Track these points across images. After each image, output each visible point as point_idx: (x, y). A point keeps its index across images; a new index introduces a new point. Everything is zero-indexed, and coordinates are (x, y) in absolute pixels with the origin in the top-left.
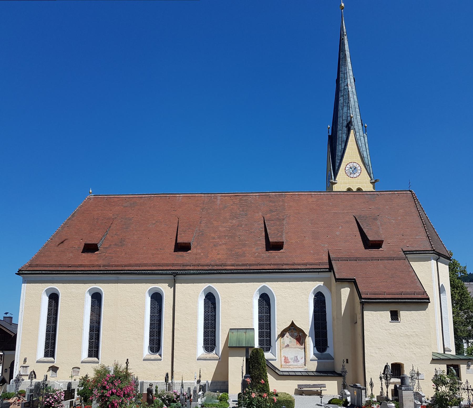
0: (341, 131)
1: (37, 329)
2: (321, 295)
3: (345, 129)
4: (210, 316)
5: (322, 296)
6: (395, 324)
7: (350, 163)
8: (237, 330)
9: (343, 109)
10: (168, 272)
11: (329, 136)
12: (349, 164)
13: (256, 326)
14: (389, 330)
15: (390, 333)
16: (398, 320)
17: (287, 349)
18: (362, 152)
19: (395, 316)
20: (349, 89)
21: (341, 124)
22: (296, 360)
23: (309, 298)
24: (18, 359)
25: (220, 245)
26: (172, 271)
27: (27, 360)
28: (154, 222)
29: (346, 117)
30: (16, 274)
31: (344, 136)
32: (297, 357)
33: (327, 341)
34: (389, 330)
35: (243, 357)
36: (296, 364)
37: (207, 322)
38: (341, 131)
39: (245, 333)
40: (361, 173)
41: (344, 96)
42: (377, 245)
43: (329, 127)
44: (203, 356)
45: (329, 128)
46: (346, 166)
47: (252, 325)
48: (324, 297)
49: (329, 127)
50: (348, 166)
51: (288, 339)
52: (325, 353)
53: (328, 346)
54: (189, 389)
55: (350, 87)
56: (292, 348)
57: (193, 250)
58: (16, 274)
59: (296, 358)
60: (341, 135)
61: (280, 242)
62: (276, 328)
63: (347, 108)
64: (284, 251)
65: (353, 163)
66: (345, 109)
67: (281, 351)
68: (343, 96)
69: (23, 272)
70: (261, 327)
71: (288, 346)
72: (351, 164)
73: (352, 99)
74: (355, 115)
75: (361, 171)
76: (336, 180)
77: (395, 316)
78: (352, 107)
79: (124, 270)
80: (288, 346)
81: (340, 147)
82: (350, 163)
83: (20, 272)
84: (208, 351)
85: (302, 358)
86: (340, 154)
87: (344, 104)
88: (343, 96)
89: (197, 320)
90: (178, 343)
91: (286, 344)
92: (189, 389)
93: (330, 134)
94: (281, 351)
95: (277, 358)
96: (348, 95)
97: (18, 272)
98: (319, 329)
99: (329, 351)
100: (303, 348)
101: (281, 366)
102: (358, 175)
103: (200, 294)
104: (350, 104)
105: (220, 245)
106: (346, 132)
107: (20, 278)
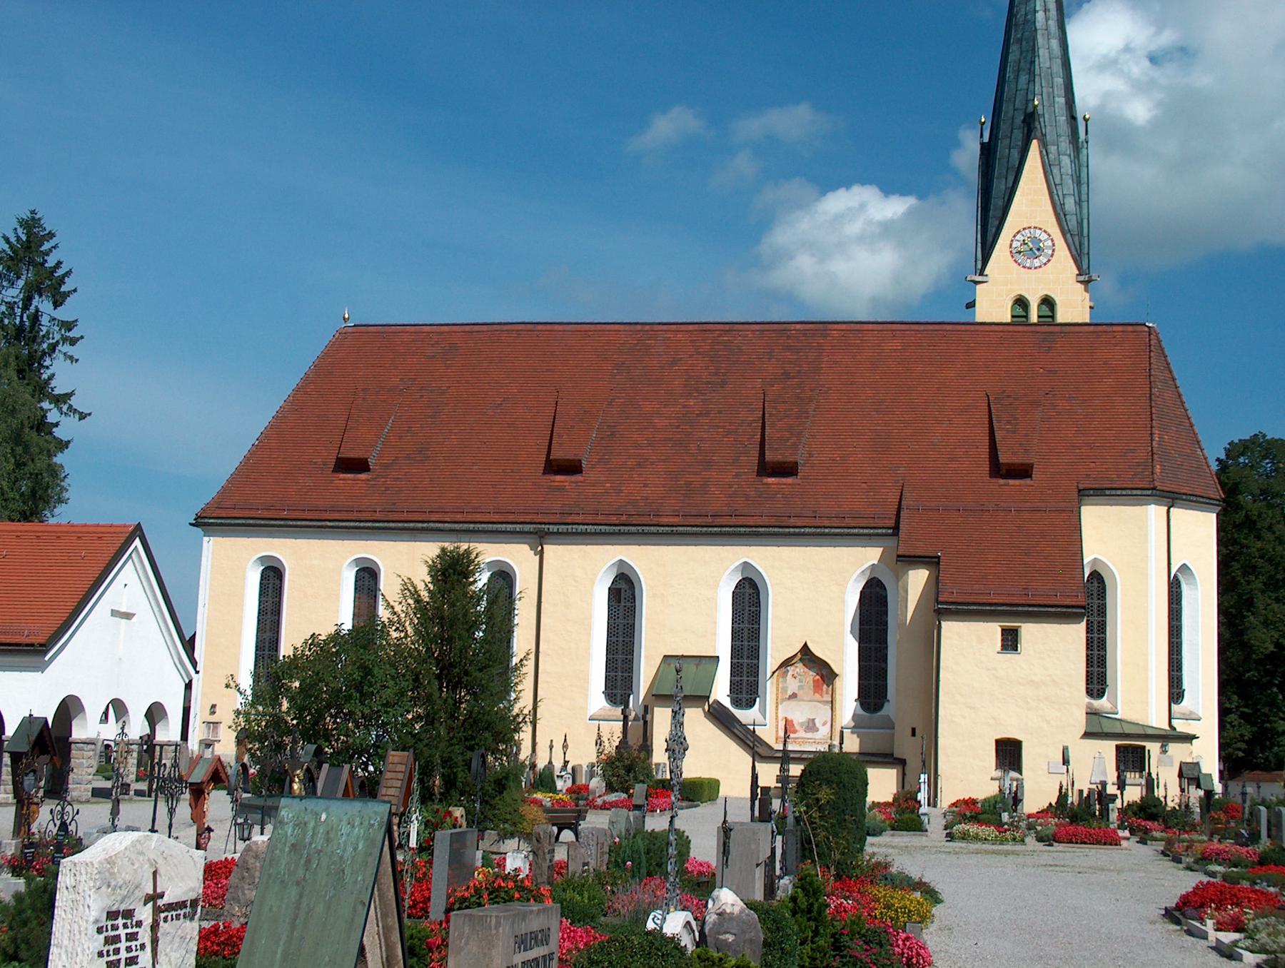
0: (1008, 140)
1: (237, 645)
2: (878, 585)
3: (1018, 135)
4: (622, 625)
5: (881, 588)
6: (1010, 657)
7: (1024, 229)
8: (698, 659)
9: (1017, 78)
10: (527, 528)
11: (982, 144)
12: (1023, 233)
13: (723, 648)
14: (996, 669)
15: (997, 677)
16: (1017, 650)
17: (793, 703)
18: (1061, 198)
19: (1010, 641)
20: (1037, 24)
21: (1010, 121)
22: (811, 726)
23: (97, 757)
24: (199, 706)
25: (652, 463)
26: (534, 526)
27: (217, 709)
28: (499, 401)
29: (1024, 102)
30: (191, 524)
31: (1015, 154)
32: (814, 720)
33: (886, 687)
34: (996, 669)
35: (290, 643)
36: (809, 735)
37: (614, 639)
38: (1007, 141)
39: (697, 665)
40: (1052, 255)
41: (1024, 43)
42: (1023, 472)
43: (983, 120)
44: (602, 713)
45: (984, 123)
46: (1015, 236)
47: (714, 648)
48: (885, 589)
49: (983, 120)
50: (1018, 237)
51: (801, 677)
52: (879, 714)
53: (888, 698)
54: (59, 264)
55: (1040, 16)
56: (803, 701)
57: (589, 475)
58: (191, 524)
59: (811, 725)
60: (1007, 150)
61: (790, 462)
62: (769, 657)
63: (1027, 76)
64: (799, 481)
65: (1032, 230)
66: (1023, 78)
67: (777, 707)
68: (1020, 41)
69: (206, 520)
70: (736, 652)
71: (794, 696)
72: (1027, 231)
73: (1043, 52)
74: (1049, 97)
75: (1054, 250)
76: (985, 273)
77: (1010, 641)
78: (1042, 75)
79: (429, 522)
80: (794, 696)
81: (1004, 182)
82: (1024, 229)
83: (199, 520)
84: (615, 703)
85: (824, 724)
86: (1000, 203)
87: (1022, 64)
88: (1020, 41)
89: (589, 634)
90: (547, 682)
91: (790, 693)
92: (59, 264)
93: (986, 139)
94: (777, 707)
95: (768, 721)
96: (1034, 39)
97: (195, 519)
98: (870, 660)
99: (889, 709)
100: (827, 702)
101: (777, 739)
102: (1045, 260)
103: (599, 577)
104: (1037, 67)
105: (652, 463)
106: (1020, 143)
107: (199, 530)
